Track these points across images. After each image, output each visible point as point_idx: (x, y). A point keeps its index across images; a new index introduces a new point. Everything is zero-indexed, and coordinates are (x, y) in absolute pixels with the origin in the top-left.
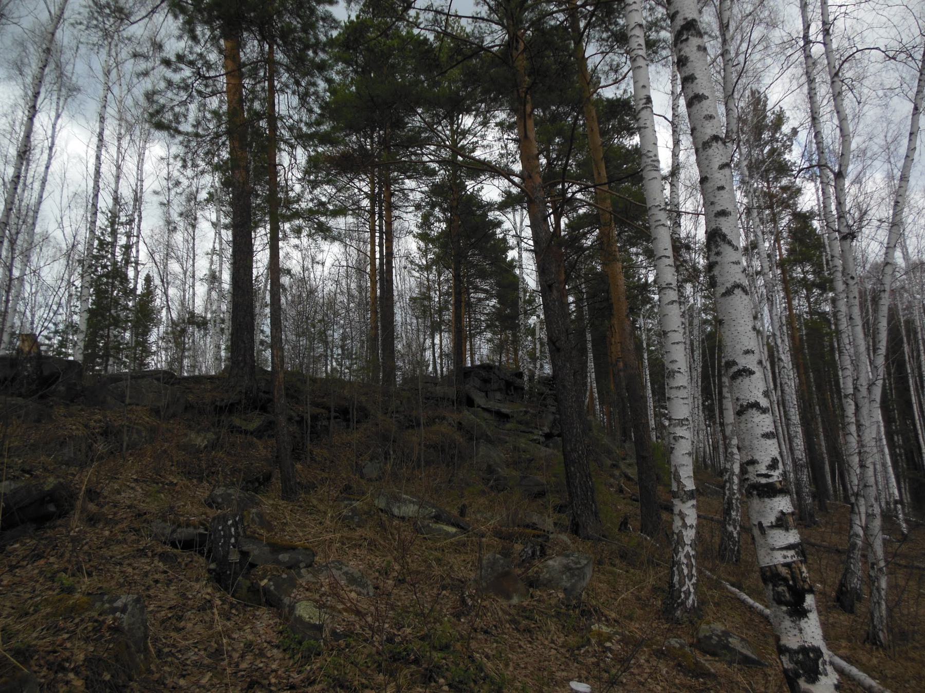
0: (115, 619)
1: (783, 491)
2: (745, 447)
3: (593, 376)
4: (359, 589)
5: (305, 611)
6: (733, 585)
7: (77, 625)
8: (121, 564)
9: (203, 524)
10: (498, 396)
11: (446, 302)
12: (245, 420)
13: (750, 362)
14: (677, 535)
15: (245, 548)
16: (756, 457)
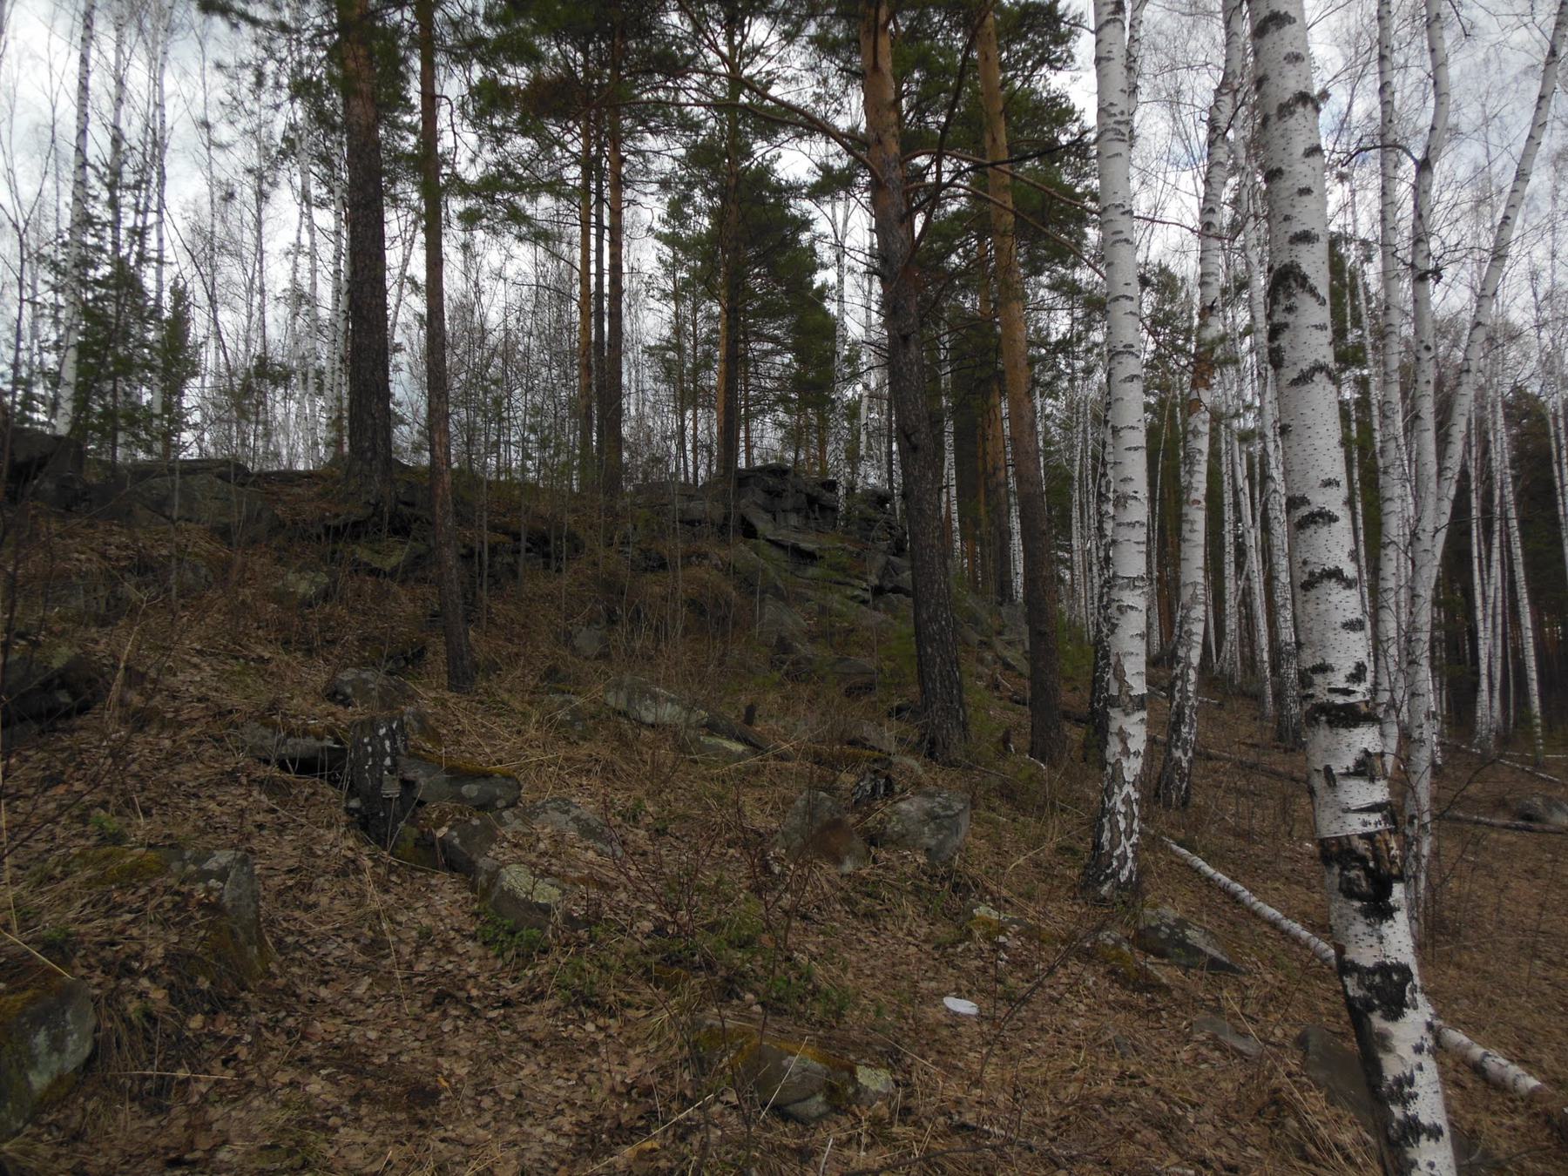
0: (209, 891)
1: (1370, 718)
2: (1312, 644)
3: (953, 491)
4: (599, 845)
5: (516, 878)
6: (1181, 844)
7: (145, 898)
8: (196, 796)
9: (332, 733)
10: (794, 520)
11: (708, 355)
12: (378, 552)
13: (1333, 500)
14: (1113, 765)
15: (410, 775)
16: (1330, 661)
